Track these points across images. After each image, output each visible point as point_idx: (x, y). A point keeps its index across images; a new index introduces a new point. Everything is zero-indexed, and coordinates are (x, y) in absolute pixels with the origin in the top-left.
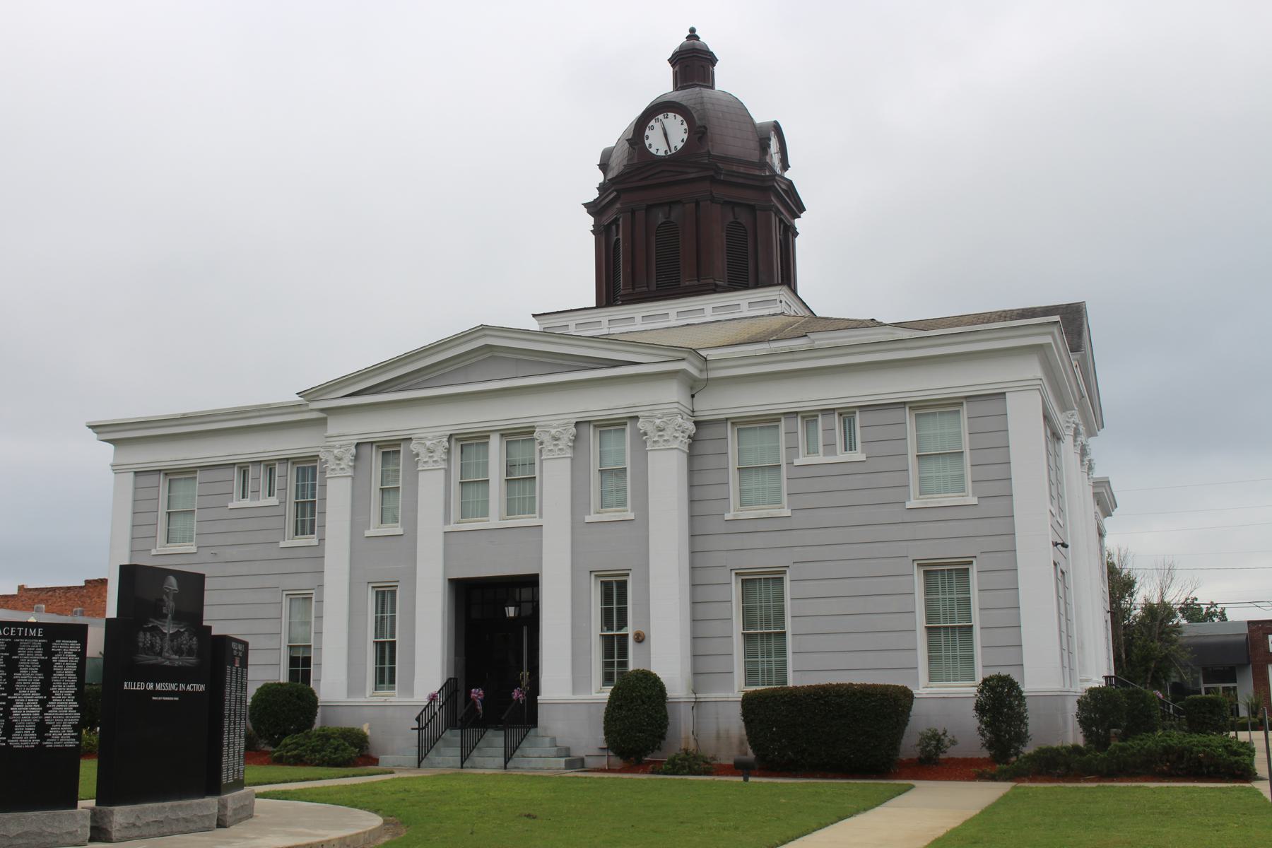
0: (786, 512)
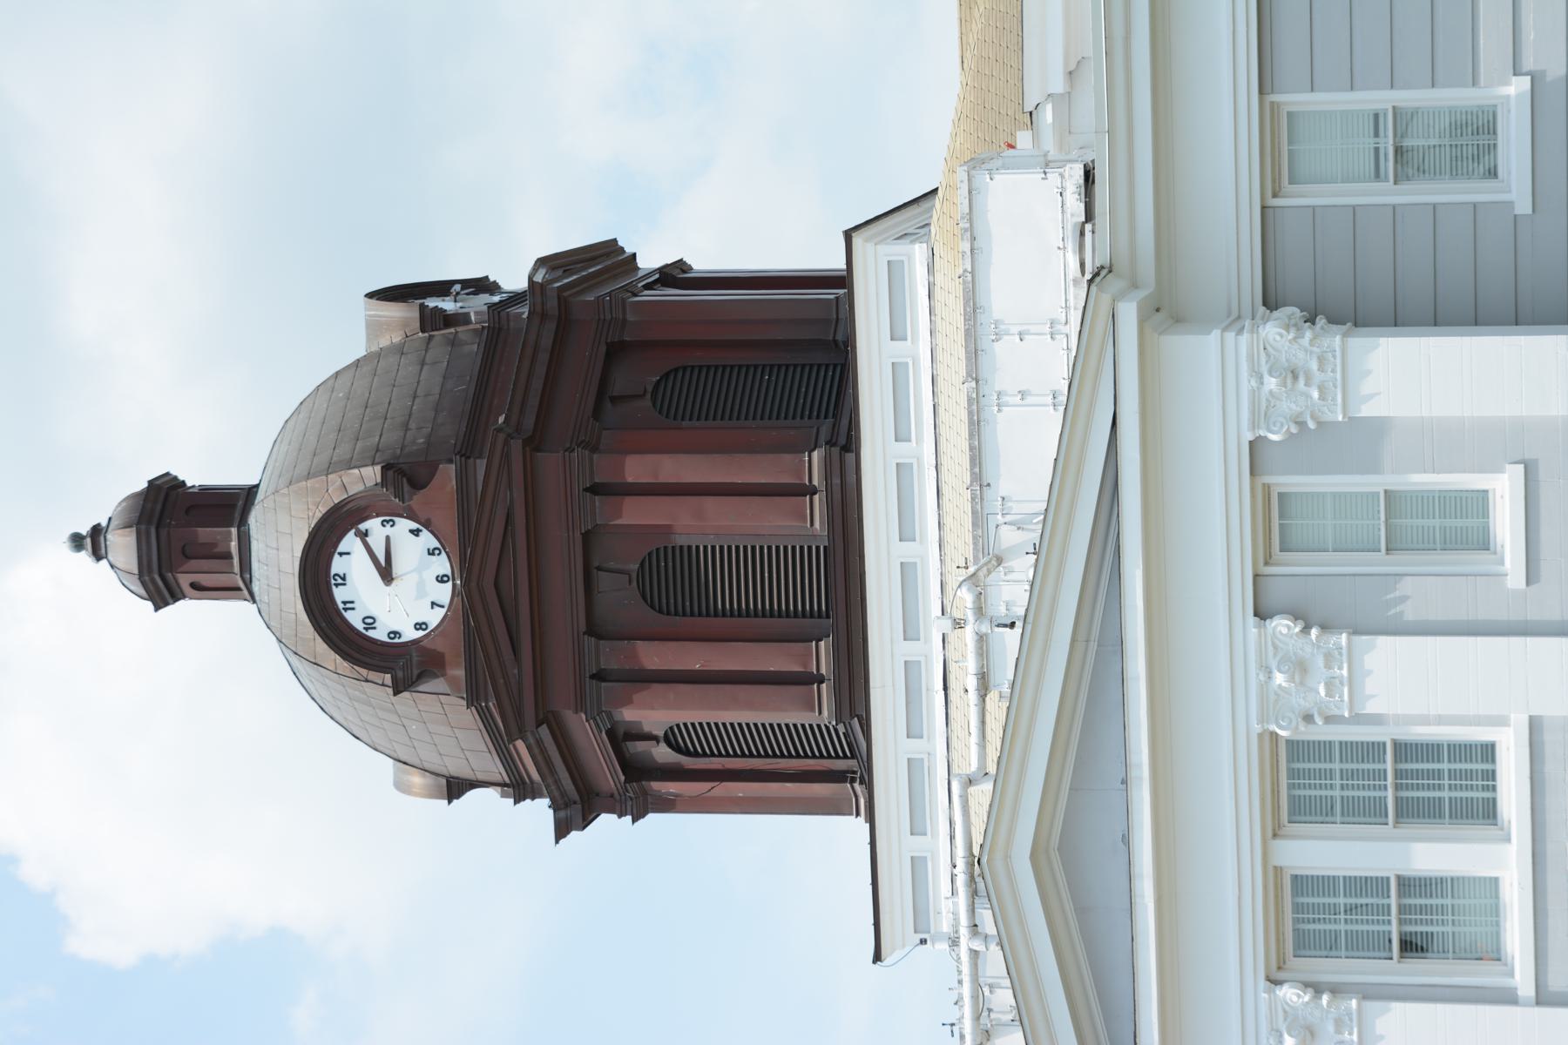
0: (1518, 88)
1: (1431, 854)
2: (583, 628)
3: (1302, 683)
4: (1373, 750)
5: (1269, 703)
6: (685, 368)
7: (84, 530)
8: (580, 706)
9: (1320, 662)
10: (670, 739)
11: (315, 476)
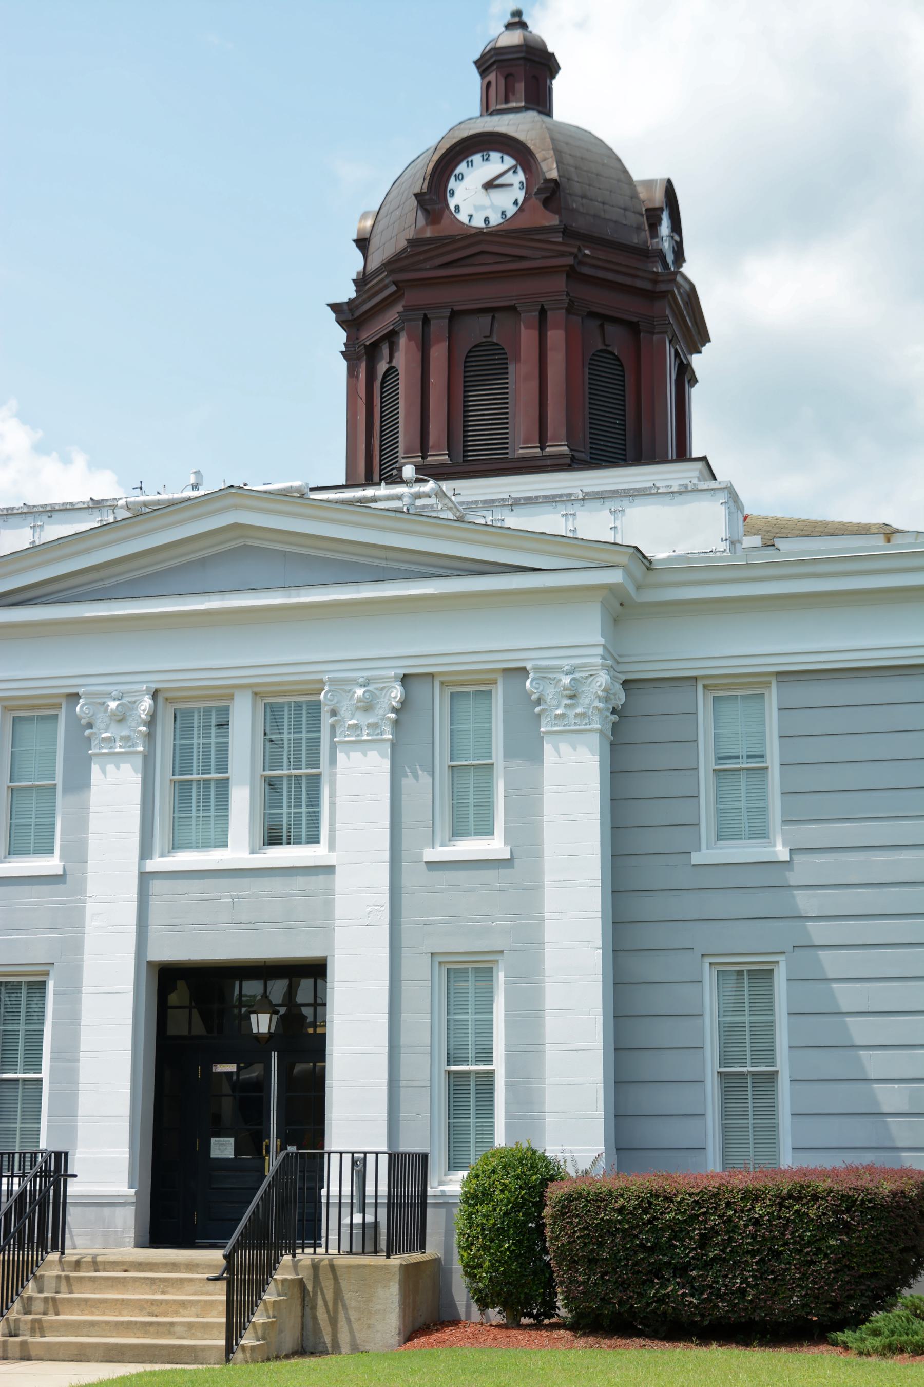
0: (781, 852)
1: (242, 801)
2: (456, 308)
3: (357, 708)
4: (314, 762)
5: (343, 685)
6: (623, 371)
7: (525, 18)
8: (407, 309)
9: (371, 721)
10: (391, 370)
11: (553, 143)
